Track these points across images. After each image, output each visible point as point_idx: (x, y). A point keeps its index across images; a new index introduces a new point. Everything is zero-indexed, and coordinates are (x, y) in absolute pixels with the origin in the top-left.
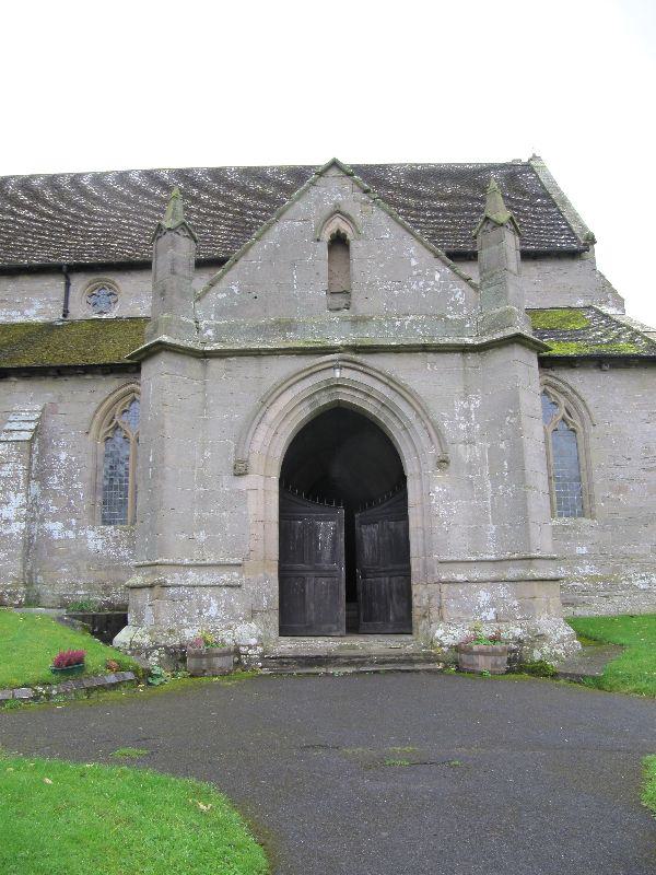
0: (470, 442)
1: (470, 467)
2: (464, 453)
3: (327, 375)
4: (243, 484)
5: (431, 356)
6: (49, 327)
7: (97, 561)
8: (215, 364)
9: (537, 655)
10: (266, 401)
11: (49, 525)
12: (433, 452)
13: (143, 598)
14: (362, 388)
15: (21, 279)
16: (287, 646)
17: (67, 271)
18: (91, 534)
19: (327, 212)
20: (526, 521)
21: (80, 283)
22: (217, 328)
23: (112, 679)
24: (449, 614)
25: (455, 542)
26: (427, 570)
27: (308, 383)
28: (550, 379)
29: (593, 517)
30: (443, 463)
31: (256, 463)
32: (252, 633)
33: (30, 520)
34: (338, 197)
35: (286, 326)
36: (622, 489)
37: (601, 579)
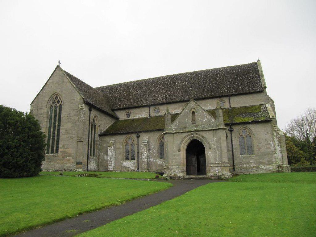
0: (214, 145)
1: (214, 149)
2: (214, 147)
3: (191, 136)
4: (180, 153)
5: (208, 131)
6: (146, 118)
7: (159, 165)
8: (175, 135)
9: (222, 177)
10: (183, 140)
11: (151, 159)
12: (208, 147)
13: (166, 170)
14: (198, 137)
15: (141, 108)
16: (187, 177)
17: (149, 106)
18: (158, 161)
19: (191, 108)
20: (222, 157)
21: (152, 108)
22: (175, 129)
23: (162, 179)
24: (211, 171)
25: (212, 161)
26: (208, 165)
27: (189, 137)
28: (246, 127)
29: (254, 154)
30: (210, 148)
31: (182, 149)
32: (181, 175)
33: (147, 158)
34: (193, 105)
35: (185, 128)
36: (260, 149)
37: (256, 167)
